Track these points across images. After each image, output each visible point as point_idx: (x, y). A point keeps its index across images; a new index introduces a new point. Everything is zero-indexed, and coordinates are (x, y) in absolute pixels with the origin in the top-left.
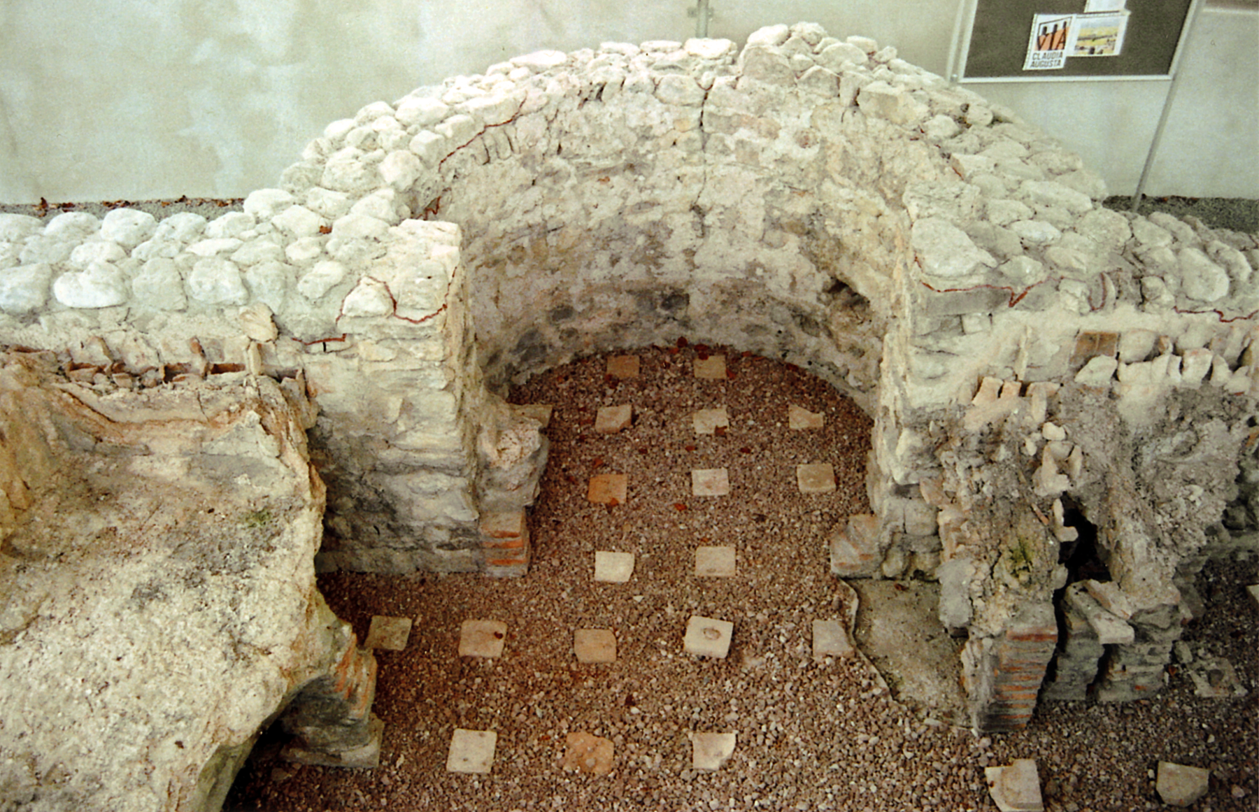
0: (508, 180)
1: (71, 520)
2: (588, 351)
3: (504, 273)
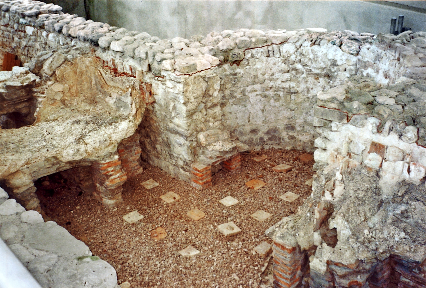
0: (277, 67)
1: (83, 104)
2: (298, 148)
3: (269, 102)
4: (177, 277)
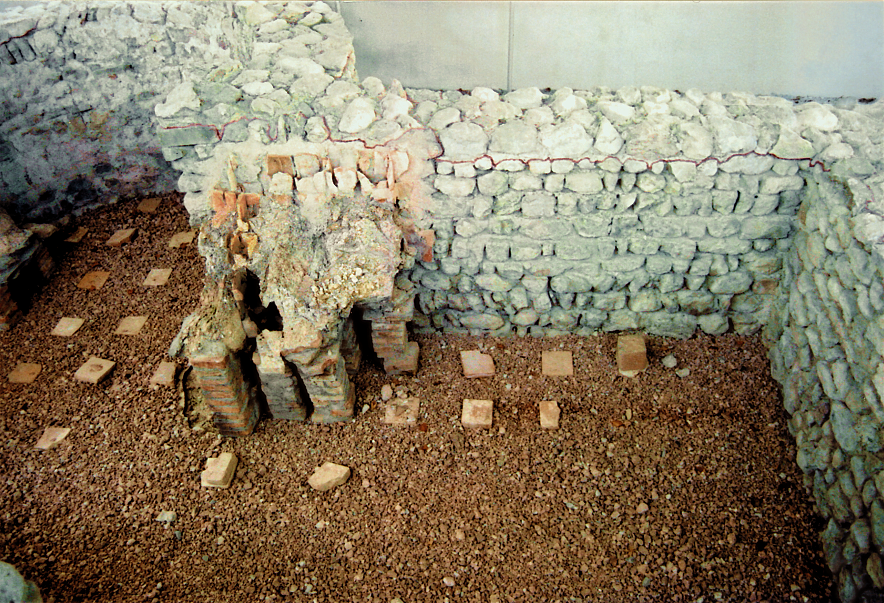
4: (58, 487)
